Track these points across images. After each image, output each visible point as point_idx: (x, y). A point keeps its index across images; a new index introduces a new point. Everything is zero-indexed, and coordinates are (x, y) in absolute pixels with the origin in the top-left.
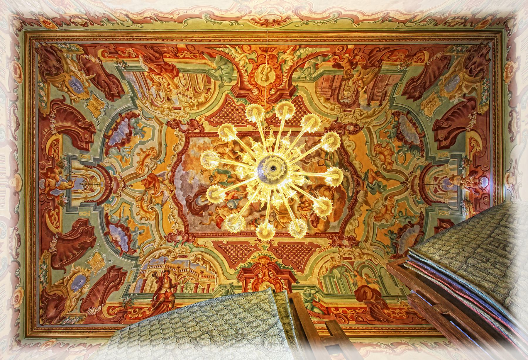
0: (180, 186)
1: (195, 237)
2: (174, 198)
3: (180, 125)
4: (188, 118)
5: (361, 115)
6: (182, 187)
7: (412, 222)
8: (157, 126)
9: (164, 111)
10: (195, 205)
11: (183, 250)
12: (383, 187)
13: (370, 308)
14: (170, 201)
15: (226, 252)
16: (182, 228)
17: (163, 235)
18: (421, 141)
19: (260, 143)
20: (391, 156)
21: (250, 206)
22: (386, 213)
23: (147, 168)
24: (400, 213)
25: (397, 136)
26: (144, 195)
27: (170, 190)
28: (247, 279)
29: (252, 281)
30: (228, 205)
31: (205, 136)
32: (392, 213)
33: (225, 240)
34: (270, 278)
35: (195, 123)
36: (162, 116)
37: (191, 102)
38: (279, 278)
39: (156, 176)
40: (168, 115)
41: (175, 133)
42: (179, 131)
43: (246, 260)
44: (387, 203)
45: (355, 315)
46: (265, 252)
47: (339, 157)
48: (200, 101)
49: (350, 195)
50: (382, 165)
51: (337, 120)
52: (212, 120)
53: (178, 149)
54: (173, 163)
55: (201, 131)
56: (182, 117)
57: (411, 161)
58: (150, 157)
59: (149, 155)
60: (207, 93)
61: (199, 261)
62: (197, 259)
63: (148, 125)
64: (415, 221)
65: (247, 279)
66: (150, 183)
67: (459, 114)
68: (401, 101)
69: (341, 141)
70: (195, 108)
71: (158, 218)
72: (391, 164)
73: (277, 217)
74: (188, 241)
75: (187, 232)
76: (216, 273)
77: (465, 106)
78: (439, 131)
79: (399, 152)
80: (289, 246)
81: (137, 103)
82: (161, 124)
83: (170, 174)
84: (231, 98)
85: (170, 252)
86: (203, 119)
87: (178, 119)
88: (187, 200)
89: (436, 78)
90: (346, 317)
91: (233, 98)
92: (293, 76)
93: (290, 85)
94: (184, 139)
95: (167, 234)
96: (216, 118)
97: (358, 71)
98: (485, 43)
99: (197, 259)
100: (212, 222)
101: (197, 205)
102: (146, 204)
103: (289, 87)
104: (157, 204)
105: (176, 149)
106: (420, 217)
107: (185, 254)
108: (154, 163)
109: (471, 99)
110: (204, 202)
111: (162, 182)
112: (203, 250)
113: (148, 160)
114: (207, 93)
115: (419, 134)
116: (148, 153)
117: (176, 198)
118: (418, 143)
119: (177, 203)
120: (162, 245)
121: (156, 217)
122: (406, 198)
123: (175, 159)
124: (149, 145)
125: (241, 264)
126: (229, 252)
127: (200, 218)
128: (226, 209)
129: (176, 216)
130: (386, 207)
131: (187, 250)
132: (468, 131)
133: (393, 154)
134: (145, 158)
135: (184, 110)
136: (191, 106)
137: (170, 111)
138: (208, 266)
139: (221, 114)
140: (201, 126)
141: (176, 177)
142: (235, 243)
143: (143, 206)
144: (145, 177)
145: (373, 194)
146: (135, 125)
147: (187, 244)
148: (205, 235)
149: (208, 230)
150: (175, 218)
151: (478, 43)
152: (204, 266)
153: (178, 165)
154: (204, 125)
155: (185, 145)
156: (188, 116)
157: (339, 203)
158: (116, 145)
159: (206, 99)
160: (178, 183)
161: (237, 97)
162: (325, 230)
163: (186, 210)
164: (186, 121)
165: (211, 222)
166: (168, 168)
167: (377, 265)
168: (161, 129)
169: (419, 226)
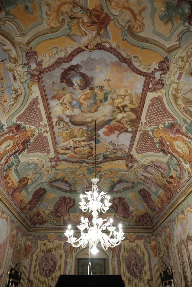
0: (93, 57)
1: (38, 82)
2: (79, 51)
3: (161, 72)
4: (167, 82)
5: (137, 171)
6: (91, 59)
7: (71, 186)
8: (168, 45)
9: (182, 61)
10: (73, 74)
11: (21, 75)
12: (91, 174)
13: (17, 188)
14: (76, 46)
15: (30, 110)
16: (45, 65)
17: (32, 44)
18: (115, 191)
19: (184, 215)
20: (109, 177)
21: (93, 225)
22: (75, 175)
23: (117, 13)
24: (76, 181)
25: (121, 181)
26: (81, 8)
27: (88, 45)
28: (11, 131)
29: (11, 134)
30: (138, 83)
31: (143, 91)
32: (75, 178)
33: (41, 106)
34: (17, 141)
35: (159, 86)
36: (177, 56)
37: (181, 92)
38: (19, 146)
39: (106, 26)
40: (176, 63)
41: (154, 63)
42: (155, 69)
43: (27, 124)
44: (81, 176)
45: (10, 187)
46: (37, 131)
47: (112, 157)
48: (179, 100)
49: (85, 161)
50: (104, 173)
51: (137, 161)
52: (158, 100)
53: (136, 61)
54: (120, 51)
55: (149, 89)
56: (169, 78)
57: (105, 187)
58: (133, 21)
59: (135, 19)
60: (183, 108)
61: (15, 93)
62: (16, 91)
63: (175, 31)
64: (72, 188)
65: (11, 131)
66: (98, 17)
67: (124, 210)
68: (141, 187)
69: (27, 205)
70: (174, 92)
71: (52, 32)
72: (105, 177)
73: (67, 131)
74: (33, 76)
75: (41, 72)
76: (8, 111)
77: (127, 212)
78: (118, 200)
79: (111, 181)
80: (33, 151)
81: (33, 165)
82: (170, 50)
83: (108, 46)
84: (173, 120)
85: (15, 60)
86: (161, 94)
87: (169, 72)
88: (77, 66)
89: (147, 203)
90: (7, 185)
91: (173, 122)
92: (154, 192)
93: (169, 153)
94: (145, 71)
95: (35, 50)
96: (159, 104)
97: (165, 181)
98: (152, 225)
99: (16, 91)
100: (56, 92)
101: (72, 76)
102: (68, 10)
103: (168, 152)
104: (70, 28)
105: (136, 59)
106: (75, 190)
107: (17, 78)
108: (124, 24)
109: (129, 216)
110: (76, 82)
111: (98, 34)
112: (26, 93)
113: (128, 16)
114: (183, 108)
115: (119, 191)
116: (138, 18)
117: (79, 52)
118: (114, 190)
119: (73, 55)
120: (20, 47)
121: (53, 28)
122: (84, 184)
123: (124, 54)
124: (147, 22)
125: (23, 123)
126: (31, 112)
127: (59, 81)
128: (70, 100)
129: (57, 56)
130: (79, 175)
131: (23, 78)
132: (114, 214)
133: (110, 178)
134: (132, 12)
135: (175, 82)
136: (177, 90)
137: (180, 68)
138: (13, 102)
139: (27, 113)
140: (155, 90)
141: (104, 52)
142: (148, 111)
143: (66, 6)
144: (106, 11)
145: (87, 170)
146: (180, 11)
147: (29, 76)
148: (42, 90)
149: (47, 91)
150: (55, 55)
151: (154, 223)
152: (12, 100)
153: (117, 56)
154: (154, 93)
155: (137, 70)
156: (168, 84)
157: (80, 157)
158: (95, 167)
159: (179, 105)
160: (97, 54)
161: (172, 124)
162: (60, 154)
163: (66, 66)
164: (163, 79)
165: (56, 91)
166: (115, 43)
167: (43, 177)
168: (163, 49)
169: (70, 189)
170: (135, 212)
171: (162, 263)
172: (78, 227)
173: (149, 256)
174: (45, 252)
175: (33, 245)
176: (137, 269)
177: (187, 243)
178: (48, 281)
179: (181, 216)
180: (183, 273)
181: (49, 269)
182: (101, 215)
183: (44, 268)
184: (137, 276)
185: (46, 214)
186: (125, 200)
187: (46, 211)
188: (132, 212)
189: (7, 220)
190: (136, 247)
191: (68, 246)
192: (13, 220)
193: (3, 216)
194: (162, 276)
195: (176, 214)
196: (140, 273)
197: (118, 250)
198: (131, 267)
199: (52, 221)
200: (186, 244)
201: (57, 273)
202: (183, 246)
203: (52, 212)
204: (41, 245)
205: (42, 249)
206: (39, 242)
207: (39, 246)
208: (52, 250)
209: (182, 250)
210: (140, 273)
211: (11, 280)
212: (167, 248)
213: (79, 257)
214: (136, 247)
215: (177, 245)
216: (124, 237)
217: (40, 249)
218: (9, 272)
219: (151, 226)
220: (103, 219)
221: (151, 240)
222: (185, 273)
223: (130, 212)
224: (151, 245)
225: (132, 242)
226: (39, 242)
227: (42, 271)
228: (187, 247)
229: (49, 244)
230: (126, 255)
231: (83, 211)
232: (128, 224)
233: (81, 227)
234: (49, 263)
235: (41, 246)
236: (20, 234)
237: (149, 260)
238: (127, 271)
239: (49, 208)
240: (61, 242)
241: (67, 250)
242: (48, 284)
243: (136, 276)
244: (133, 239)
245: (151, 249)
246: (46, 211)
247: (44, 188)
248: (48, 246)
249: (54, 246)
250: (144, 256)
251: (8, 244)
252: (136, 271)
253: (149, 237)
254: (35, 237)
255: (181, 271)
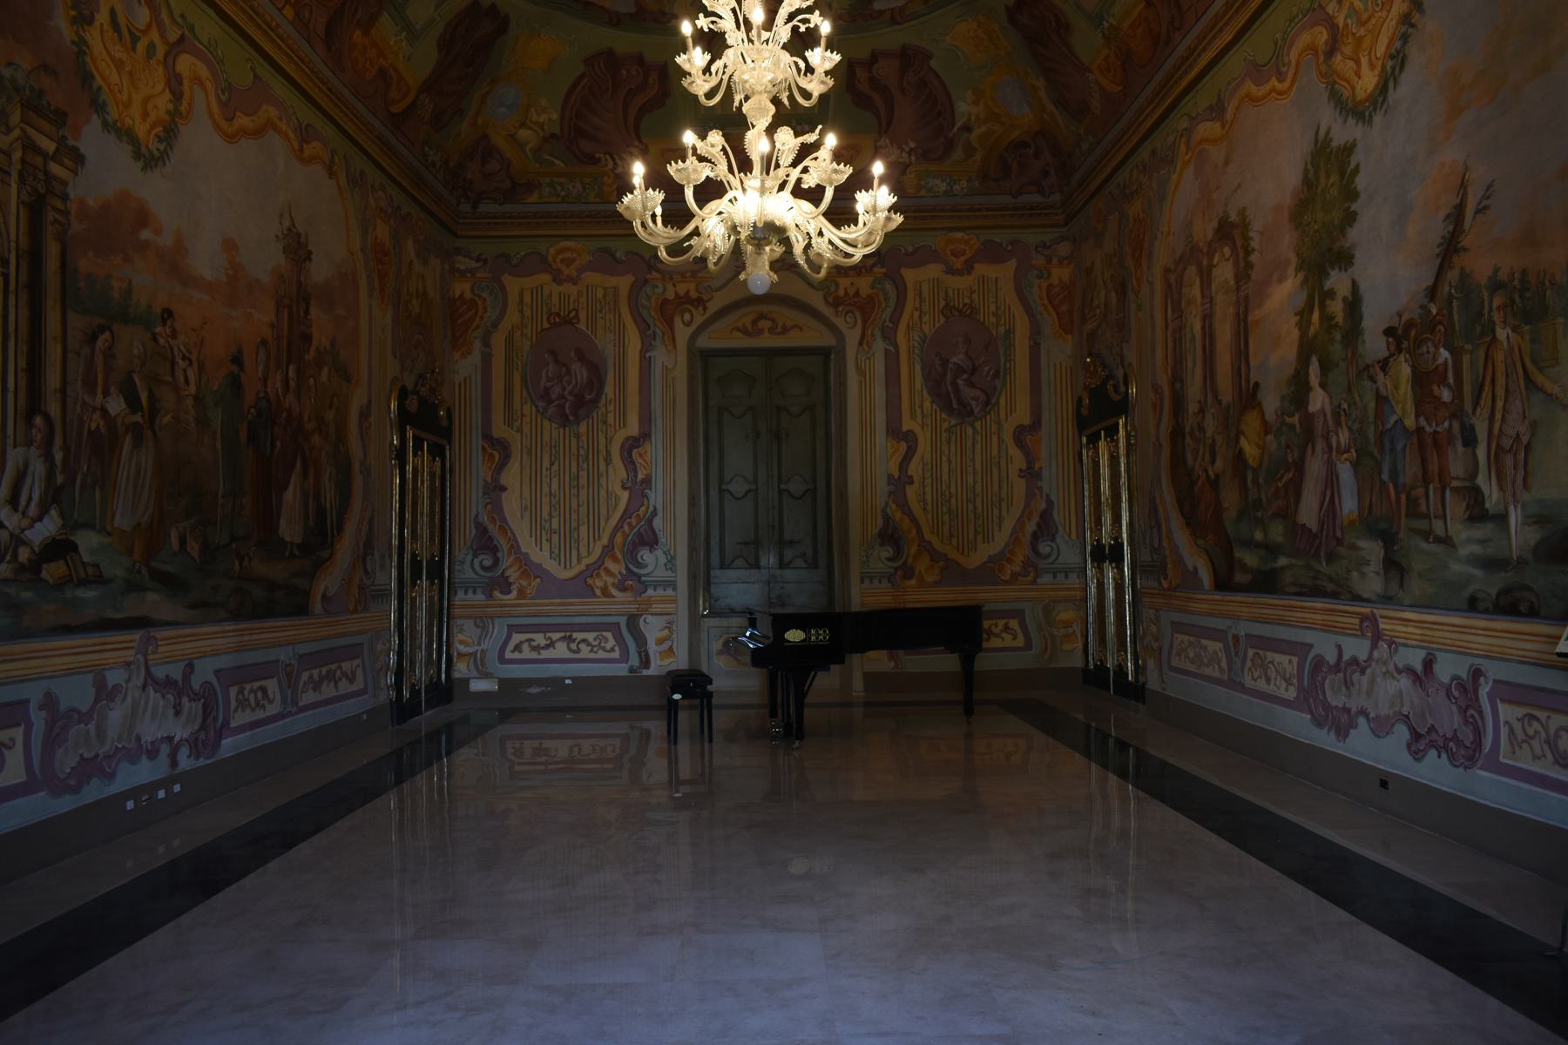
18: (882, 12)
19: (1218, 124)
169: (633, 10)
170: (983, 129)
171: (1090, 355)
172: (672, 169)
173: (1036, 331)
174: (546, 325)
175: (485, 295)
176: (971, 384)
177: (1210, 255)
178: (574, 441)
179: (1208, 128)
180: (1172, 384)
181: (571, 393)
182: (790, 115)
183: (547, 390)
184: (971, 413)
185: (527, 148)
186: (933, 63)
187: (523, 134)
188: (967, 128)
189: (331, 174)
190: (975, 296)
191: (649, 298)
192: (362, 172)
193: (307, 152)
194: (1085, 412)
195: (1184, 124)
196: (987, 403)
197: (889, 311)
198: (949, 377)
199: (562, 180)
200: (1205, 262)
201: (611, 408)
202: (1192, 270)
203: (553, 136)
204: (521, 295)
205: (527, 312)
206: (513, 284)
207: (513, 299)
208: (577, 316)
209: (1184, 290)
210: (987, 403)
211: (410, 434)
212: (1122, 289)
213: (704, 342)
214: (975, 296)
215: (1167, 270)
216: (899, 219)
217: (521, 311)
218: (393, 405)
219: (1057, 197)
220: (797, 135)
221: (1049, 260)
222: (1178, 386)
223: (959, 124)
224: (1050, 287)
225: (959, 273)
226: (513, 284)
227: (541, 404)
228: (1209, 273)
229: (560, 289)
230: (926, 328)
231: (703, 100)
232: (943, 187)
233: (689, 173)
234: (569, 372)
235: (521, 301)
236: (410, 243)
237: (1035, 350)
238: (925, 394)
239: (535, 118)
240: (613, 281)
241: (645, 313)
242: (574, 450)
243: (963, 412)
244: (963, 259)
245: (1046, 301)
246: (523, 134)
247: (493, 6)
248: (555, 300)
249: (583, 299)
250: (1009, 333)
251: (363, 282)
252: (968, 393)
253: (1044, 246)
254: (485, 261)
255: (1164, 381)
